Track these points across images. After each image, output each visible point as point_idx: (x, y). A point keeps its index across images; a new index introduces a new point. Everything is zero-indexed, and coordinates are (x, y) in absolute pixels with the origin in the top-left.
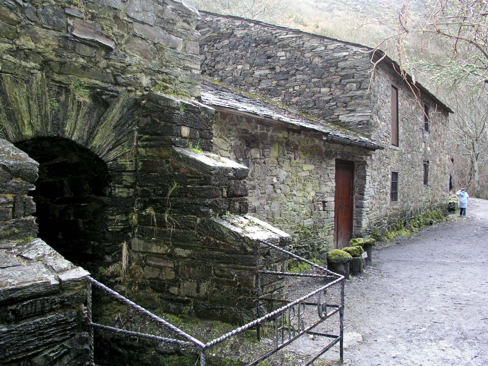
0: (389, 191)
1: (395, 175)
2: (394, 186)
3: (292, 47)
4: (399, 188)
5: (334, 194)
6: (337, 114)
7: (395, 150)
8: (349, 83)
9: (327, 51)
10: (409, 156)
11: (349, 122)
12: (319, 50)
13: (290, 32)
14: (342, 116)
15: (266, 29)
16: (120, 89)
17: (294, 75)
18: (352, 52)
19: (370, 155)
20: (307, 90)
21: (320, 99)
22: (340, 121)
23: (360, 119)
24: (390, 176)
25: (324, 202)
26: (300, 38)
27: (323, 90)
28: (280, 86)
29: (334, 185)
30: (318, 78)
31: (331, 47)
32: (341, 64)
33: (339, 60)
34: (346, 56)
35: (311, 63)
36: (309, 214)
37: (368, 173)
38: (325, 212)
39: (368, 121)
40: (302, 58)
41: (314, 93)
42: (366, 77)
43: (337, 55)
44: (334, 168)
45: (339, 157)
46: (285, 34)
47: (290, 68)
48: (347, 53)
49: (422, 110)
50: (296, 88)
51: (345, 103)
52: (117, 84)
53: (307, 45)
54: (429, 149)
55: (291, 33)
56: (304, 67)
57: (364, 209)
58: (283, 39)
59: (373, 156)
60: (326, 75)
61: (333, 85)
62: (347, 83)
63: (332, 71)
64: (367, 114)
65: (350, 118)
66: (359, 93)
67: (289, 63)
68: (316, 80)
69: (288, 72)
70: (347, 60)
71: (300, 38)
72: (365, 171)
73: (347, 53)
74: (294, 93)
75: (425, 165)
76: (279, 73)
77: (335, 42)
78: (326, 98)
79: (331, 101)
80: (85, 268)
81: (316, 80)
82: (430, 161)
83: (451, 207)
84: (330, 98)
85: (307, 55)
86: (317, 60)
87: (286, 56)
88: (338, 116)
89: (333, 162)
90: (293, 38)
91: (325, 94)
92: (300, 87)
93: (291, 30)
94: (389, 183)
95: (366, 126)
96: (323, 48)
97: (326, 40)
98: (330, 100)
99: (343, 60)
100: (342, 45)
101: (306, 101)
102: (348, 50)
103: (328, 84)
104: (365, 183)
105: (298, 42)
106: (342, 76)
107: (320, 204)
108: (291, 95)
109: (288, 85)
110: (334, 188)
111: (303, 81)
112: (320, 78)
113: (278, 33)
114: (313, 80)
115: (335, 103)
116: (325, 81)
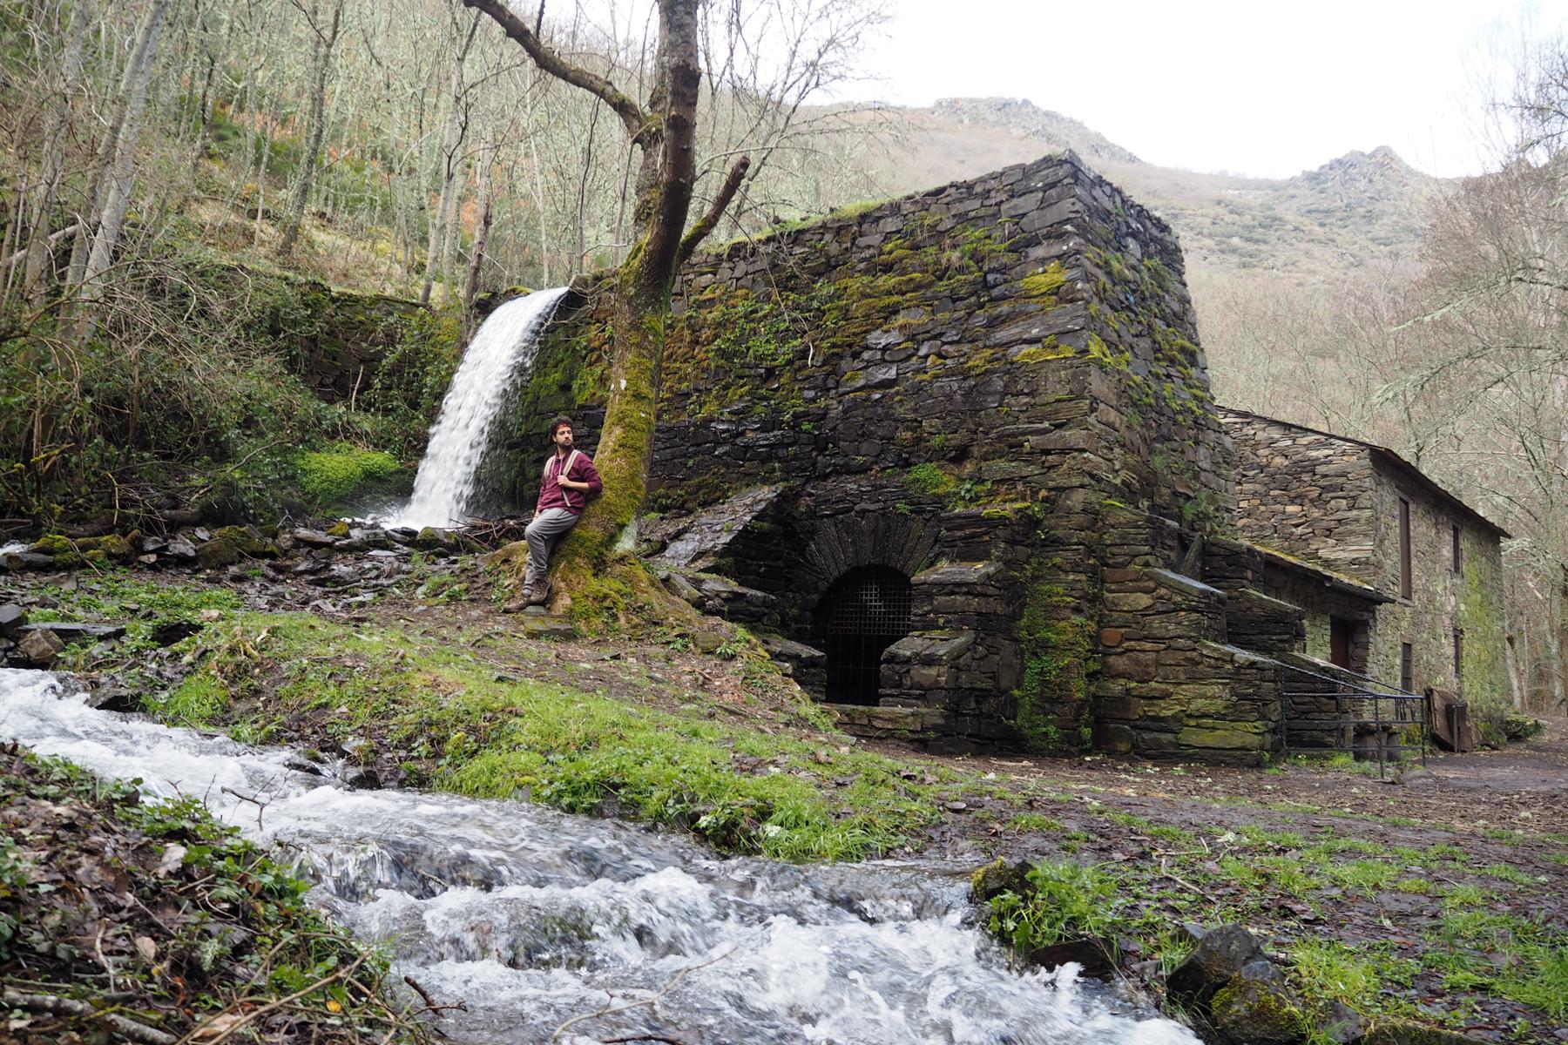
1: (1407, 647)
2: (1407, 662)
4: (1415, 671)
10: (1429, 618)
18: (1339, 451)
19: (1373, 612)
20: (1262, 508)
27: (1290, 509)
31: (1305, 441)
32: (1321, 469)
33: (1315, 462)
43: (1314, 454)
45: (1333, 612)
49: (1448, 537)
50: (1242, 504)
54: (1463, 607)
60: (1295, 484)
75: (1456, 637)
81: (1277, 492)
86: (1278, 460)
89: (1328, 619)
91: (1291, 516)
93: (1231, 411)
94: (1398, 661)
96: (1289, 442)
100: (1323, 438)
103: (1298, 499)
116: (1292, 494)
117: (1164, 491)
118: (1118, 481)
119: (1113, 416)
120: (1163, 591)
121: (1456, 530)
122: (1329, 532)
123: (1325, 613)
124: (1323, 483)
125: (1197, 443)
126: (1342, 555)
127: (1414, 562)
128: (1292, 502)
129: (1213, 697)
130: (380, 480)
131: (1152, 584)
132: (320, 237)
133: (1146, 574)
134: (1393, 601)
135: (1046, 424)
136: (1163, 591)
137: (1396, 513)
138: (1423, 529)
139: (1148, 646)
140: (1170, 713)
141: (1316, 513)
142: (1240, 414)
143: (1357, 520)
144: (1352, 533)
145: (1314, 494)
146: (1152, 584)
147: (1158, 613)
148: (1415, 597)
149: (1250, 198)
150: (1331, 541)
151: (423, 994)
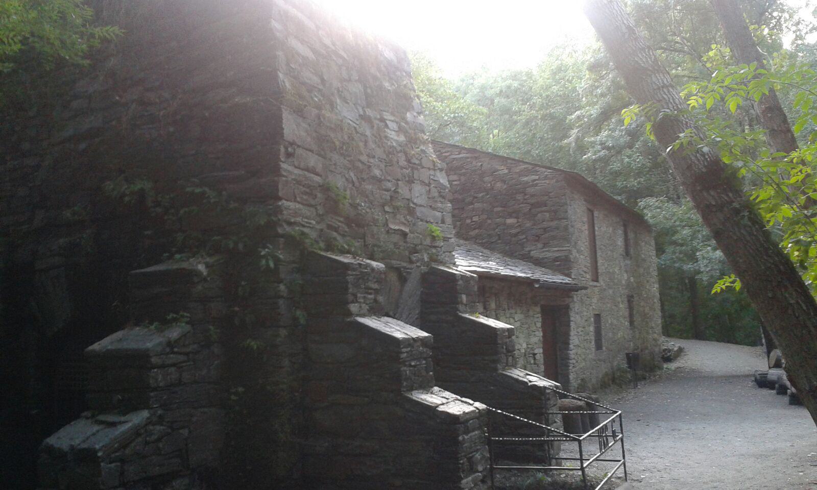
0: (593, 338)
1: (598, 317)
3: (467, 169)
4: (603, 333)
5: (541, 345)
6: (527, 249)
7: (595, 286)
8: (542, 212)
9: (512, 175)
10: (611, 291)
11: (543, 259)
12: (501, 173)
13: (463, 151)
14: (534, 252)
17: (472, 203)
19: (572, 297)
20: (489, 221)
21: (505, 231)
22: (532, 257)
23: (557, 255)
24: (592, 319)
27: (510, 221)
29: (542, 334)
30: (502, 207)
32: (531, 190)
34: (535, 180)
35: (492, 189)
37: (572, 319)
38: (536, 366)
39: (566, 257)
42: (561, 205)
43: (525, 179)
45: (542, 303)
46: (457, 153)
47: (466, 195)
51: (537, 236)
52: (411, 262)
55: (465, 152)
56: (484, 194)
57: (571, 361)
59: (575, 296)
63: (519, 198)
64: (565, 249)
65: (544, 254)
66: (554, 224)
68: (499, 209)
69: (463, 200)
70: (536, 185)
71: (476, 158)
72: (569, 317)
73: (537, 177)
74: (473, 225)
77: (521, 164)
78: (513, 231)
79: (519, 234)
81: (499, 209)
82: (635, 295)
83: (666, 356)
84: (518, 230)
86: (499, 185)
87: (460, 180)
88: (530, 251)
89: (538, 309)
90: (468, 158)
91: (511, 226)
92: (479, 217)
94: (592, 329)
95: (563, 265)
96: (506, 171)
98: (518, 233)
99: (533, 186)
101: (489, 235)
102: (539, 173)
104: (570, 330)
106: (532, 205)
107: (531, 356)
110: (541, 339)
112: (504, 207)
113: (448, 152)
115: (524, 236)
121: (625, 226)
122: (538, 238)
123: (536, 304)
124: (533, 201)
126: (549, 255)
127: (599, 253)
128: (511, 216)
132: (626, 122)
134: (586, 288)
137: (585, 219)
138: (604, 229)
141: (528, 224)
143: (557, 228)
144: (554, 238)
145: (526, 208)
148: (600, 279)
150: (540, 245)
151: (447, 252)
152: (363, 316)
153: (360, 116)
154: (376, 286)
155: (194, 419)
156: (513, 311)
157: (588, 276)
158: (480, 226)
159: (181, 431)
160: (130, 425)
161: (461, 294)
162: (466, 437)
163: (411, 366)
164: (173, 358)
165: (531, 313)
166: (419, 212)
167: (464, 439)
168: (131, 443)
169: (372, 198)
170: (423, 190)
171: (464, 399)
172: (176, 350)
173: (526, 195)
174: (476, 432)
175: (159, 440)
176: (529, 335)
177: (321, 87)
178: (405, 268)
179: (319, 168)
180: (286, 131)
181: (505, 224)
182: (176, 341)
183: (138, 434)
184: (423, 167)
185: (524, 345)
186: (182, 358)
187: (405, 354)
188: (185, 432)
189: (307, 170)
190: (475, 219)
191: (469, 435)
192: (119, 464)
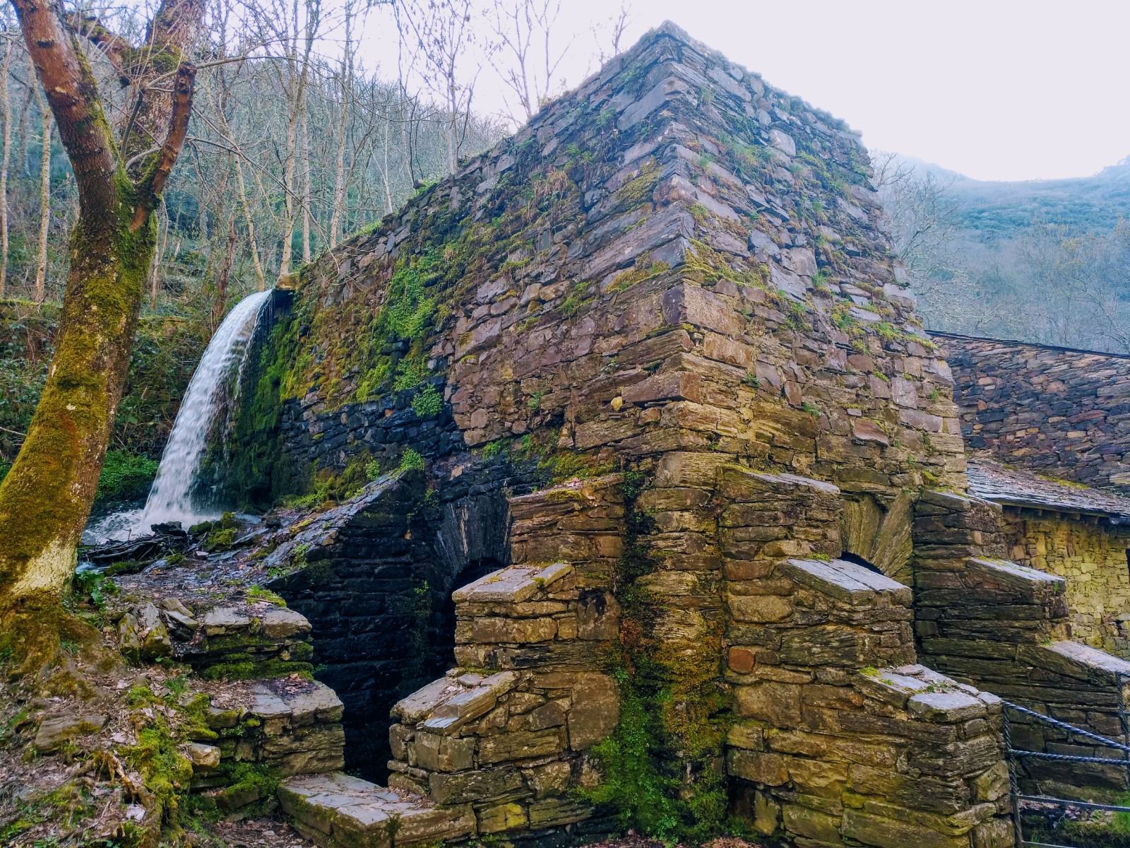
6: (1104, 473)
15: (954, 342)
16: (895, 490)
20: (1042, 436)
25: (1118, 622)
26: (1019, 352)
27: (1073, 435)
28: (989, 431)
36: (1099, 641)
40: (1024, 385)
41: (1055, 441)
43: (1094, 376)
44: (1126, 565)
48: (1114, 372)
52: (893, 485)
53: (1033, 364)
58: (987, 358)
61: (1090, 425)
62: (1120, 420)
67: (1003, 394)
69: (1002, 410)
73: (1114, 372)
76: (985, 411)
80: (339, 693)
85: (1035, 380)
88: (1108, 475)
89: (1123, 557)
93: (999, 342)
96: (1065, 367)
97: (1068, 353)
100: (1102, 358)
105: (1015, 361)
108: (1012, 447)
109: (1004, 430)
111: (1031, 423)
114: (1051, 420)
117: (834, 440)
118: (750, 435)
119: (732, 348)
120: (801, 594)
125: (891, 374)
129: (882, 764)
130: (122, 497)
131: (786, 583)
133: (779, 568)
135: (639, 369)
136: (801, 594)
139: (788, 675)
140: (822, 783)
142: (1006, 343)
145: (1099, 415)
146: (786, 583)
147: (797, 627)
149: (1059, 193)
152: (804, 557)
153: (809, 290)
154: (824, 516)
155: (578, 687)
156: (1080, 558)
157: (285, 272)
158: (1028, 443)
159: (559, 702)
160: (487, 689)
161: (972, 530)
162: (962, 746)
163: (872, 631)
164: (547, 607)
165: (1109, 562)
166: (904, 417)
167: (957, 748)
168: (488, 713)
169: (827, 397)
170: (911, 386)
171: (962, 686)
172: (551, 596)
173: (1097, 397)
174: (982, 739)
175: (528, 712)
176: (1109, 594)
177: (748, 254)
178: (883, 493)
179: (741, 358)
180: (690, 311)
181: (1066, 439)
182: (550, 585)
183: (498, 703)
184: (910, 355)
185: (1100, 608)
186: (559, 607)
187: (861, 615)
188: (564, 704)
189: (723, 360)
190: (1019, 434)
191: (969, 742)
192: (472, 739)
